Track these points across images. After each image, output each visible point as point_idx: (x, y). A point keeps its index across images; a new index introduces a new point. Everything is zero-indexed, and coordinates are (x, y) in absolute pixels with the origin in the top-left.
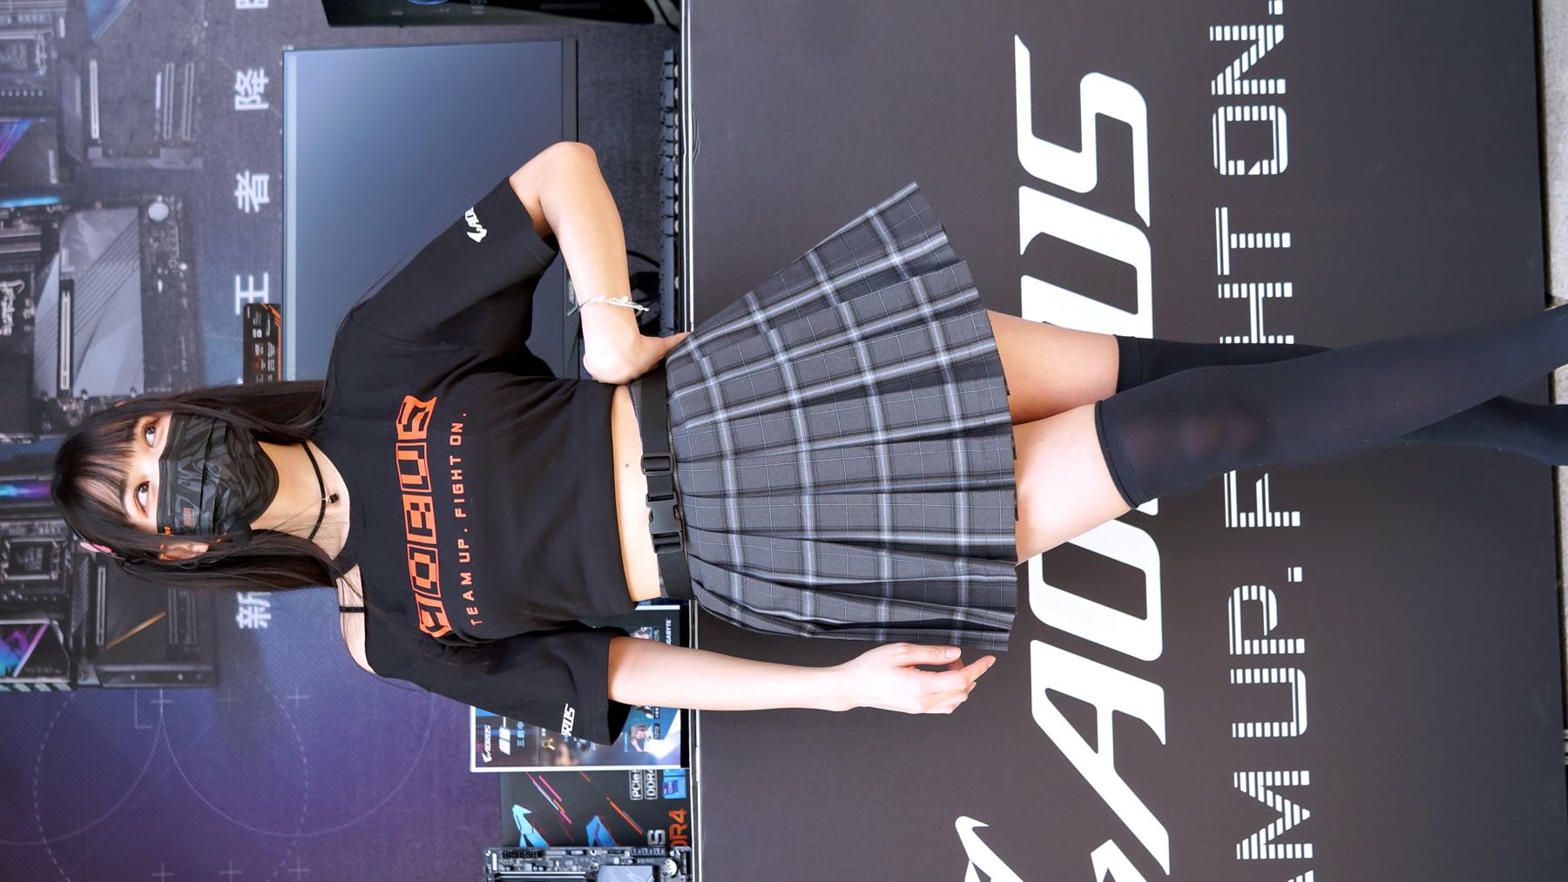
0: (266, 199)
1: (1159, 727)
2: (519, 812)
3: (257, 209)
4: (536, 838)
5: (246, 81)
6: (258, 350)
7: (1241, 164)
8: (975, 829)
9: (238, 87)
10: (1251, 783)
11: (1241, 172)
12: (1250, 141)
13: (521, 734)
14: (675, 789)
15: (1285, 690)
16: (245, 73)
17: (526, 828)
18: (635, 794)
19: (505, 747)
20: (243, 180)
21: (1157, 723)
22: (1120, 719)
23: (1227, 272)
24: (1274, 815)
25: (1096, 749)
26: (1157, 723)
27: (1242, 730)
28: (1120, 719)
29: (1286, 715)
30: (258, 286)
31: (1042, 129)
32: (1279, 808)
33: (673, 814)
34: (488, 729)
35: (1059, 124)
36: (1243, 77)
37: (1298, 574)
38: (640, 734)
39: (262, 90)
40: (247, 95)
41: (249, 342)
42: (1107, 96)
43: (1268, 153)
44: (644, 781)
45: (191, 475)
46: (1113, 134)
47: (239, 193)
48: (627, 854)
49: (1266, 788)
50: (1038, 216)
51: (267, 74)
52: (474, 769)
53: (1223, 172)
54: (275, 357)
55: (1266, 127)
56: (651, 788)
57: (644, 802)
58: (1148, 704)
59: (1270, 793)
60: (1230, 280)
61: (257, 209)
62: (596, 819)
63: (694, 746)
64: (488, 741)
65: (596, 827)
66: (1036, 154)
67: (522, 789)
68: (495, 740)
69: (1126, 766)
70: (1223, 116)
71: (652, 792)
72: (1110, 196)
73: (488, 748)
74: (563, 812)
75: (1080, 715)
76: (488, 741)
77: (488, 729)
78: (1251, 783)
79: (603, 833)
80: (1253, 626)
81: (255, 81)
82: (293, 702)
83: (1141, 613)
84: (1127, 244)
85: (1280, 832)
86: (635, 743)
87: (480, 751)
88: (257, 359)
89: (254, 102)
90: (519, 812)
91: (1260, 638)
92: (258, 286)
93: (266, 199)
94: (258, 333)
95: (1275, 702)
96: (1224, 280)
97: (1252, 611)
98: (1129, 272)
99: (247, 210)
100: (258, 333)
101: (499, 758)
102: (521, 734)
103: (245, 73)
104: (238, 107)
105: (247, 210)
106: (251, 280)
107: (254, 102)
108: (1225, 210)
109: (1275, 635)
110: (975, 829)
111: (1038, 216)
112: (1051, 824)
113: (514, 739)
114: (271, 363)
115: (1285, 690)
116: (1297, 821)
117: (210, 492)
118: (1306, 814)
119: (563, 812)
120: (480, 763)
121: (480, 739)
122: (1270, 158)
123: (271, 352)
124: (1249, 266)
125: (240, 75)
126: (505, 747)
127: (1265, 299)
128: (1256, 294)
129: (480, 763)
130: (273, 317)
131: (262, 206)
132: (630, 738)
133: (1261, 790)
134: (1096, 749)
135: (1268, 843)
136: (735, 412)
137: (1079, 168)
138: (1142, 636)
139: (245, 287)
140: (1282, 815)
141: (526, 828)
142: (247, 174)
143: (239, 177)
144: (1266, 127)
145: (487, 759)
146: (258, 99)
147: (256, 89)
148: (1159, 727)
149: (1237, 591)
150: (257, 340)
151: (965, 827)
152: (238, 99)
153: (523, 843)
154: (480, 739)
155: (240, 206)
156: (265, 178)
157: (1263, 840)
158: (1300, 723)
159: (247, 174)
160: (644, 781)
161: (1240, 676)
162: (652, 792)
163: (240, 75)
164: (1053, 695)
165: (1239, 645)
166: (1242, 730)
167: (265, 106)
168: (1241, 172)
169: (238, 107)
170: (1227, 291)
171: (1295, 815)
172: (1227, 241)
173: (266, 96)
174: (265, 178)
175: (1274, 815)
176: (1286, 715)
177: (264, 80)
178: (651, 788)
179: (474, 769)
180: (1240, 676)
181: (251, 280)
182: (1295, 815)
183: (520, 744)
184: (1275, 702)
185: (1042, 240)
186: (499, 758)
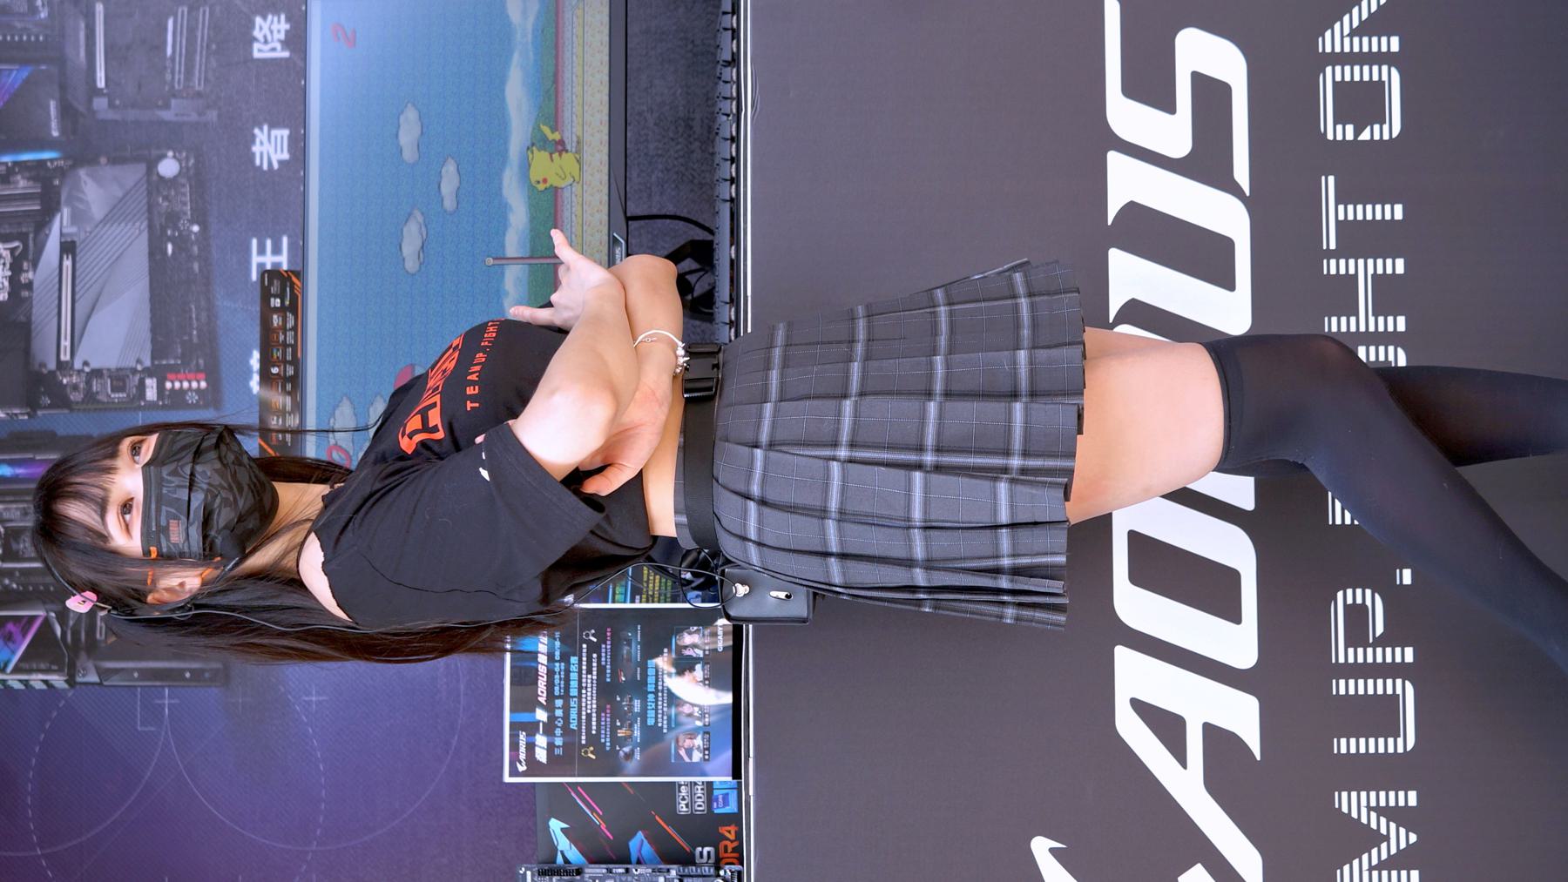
0: (286, 156)
1: (1253, 742)
2: (556, 825)
3: (276, 166)
4: (574, 855)
5: (266, 26)
6: (276, 320)
7: (1350, 128)
8: (1052, 851)
9: (256, 33)
10: (1354, 804)
11: (1350, 136)
12: (1361, 103)
13: (559, 742)
14: (726, 803)
15: (1392, 702)
16: (265, 18)
17: (563, 843)
18: (682, 808)
19: (541, 755)
20: (261, 134)
21: (1252, 738)
22: (1209, 729)
23: (1333, 246)
24: (1377, 838)
25: (1184, 764)
26: (1252, 738)
27: (1343, 746)
28: (1209, 729)
29: (1392, 728)
30: (277, 250)
31: (1130, 90)
32: (1383, 831)
33: (723, 830)
34: (522, 736)
35: (1151, 84)
36: (1353, 33)
37: (1407, 577)
38: (688, 743)
39: (282, 36)
40: (266, 42)
41: (266, 312)
42: (1203, 53)
43: (1378, 115)
44: (692, 794)
45: (176, 481)
46: (1211, 93)
47: (256, 149)
48: (673, 873)
49: (1369, 809)
50: (1126, 183)
51: (288, 20)
52: (507, 779)
53: (1330, 137)
54: (295, 328)
55: (1378, 88)
56: (700, 802)
57: (691, 817)
58: (1241, 715)
59: (1373, 815)
60: (1337, 254)
61: (276, 166)
62: (640, 835)
63: (747, 756)
64: (523, 749)
65: (639, 844)
66: (1126, 116)
67: (560, 800)
68: (531, 747)
69: (1214, 784)
70: (1330, 77)
71: (700, 805)
72: (1205, 164)
73: (522, 757)
74: (603, 826)
75: (1168, 727)
76: (523, 749)
77: (522, 736)
78: (1354, 804)
79: (647, 850)
80: (1357, 635)
81: (275, 27)
82: (309, 703)
83: (1235, 617)
84: (1224, 215)
85: (1384, 856)
86: (682, 752)
87: (514, 760)
88: (275, 331)
89: (274, 49)
90: (556, 825)
91: (1365, 645)
92: (277, 250)
93: (286, 156)
94: (276, 302)
95: (1382, 716)
96: (1330, 254)
97: (1357, 615)
98: (1227, 245)
99: (265, 167)
100: (276, 302)
101: (534, 767)
102: (559, 742)
103: (265, 18)
104: (256, 55)
105: (265, 167)
106: (269, 243)
107: (274, 49)
108: (1331, 179)
109: (1381, 642)
110: (1052, 851)
111: (1126, 183)
112: (1139, 854)
113: (551, 747)
114: (290, 335)
115: (1392, 702)
116: (1403, 845)
117: (198, 500)
118: (1413, 838)
119: (603, 826)
120: (514, 772)
121: (514, 746)
122: (1382, 123)
123: (290, 323)
124: (1357, 239)
125: (258, 20)
126: (541, 755)
127: (1375, 275)
128: (1364, 270)
129: (514, 772)
130: (293, 284)
131: (281, 162)
132: (678, 747)
133: (1364, 811)
134: (1184, 764)
135: (1371, 869)
136: (947, 459)
137: (1173, 132)
138: (1238, 644)
139: (262, 251)
140: (1387, 838)
141: (563, 843)
142: (266, 128)
143: (257, 131)
144: (1378, 88)
145: (522, 768)
146: (279, 46)
147: (276, 36)
148: (1253, 742)
149: (1340, 594)
150: (276, 310)
151: (1041, 847)
152: (256, 46)
153: (560, 860)
154: (514, 746)
155: (258, 162)
156: (286, 132)
157: (1365, 866)
158: (1409, 738)
159: (266, 128)
160: (692, 794)
161: (1342, 687)
162: (700, 805)
163: (258, 20)
164: (1139, 706)
165: (1342, 653)
166: (1343, 746)
167: (286, 54)
168: (1350, 136)
169: (256, 55)
170: (1332, 267)
171: (1401, 838)
172: (1333, 213)
173: (286, 44)
174: (286, 132)
175: (1377, 838)
176: (1392, 728)
177: (285, 26)
178: (700, 802)
179: (507, 779)
180: (1342, 687)
181: (269, 243)
182: (1401, 838)
183: (558, 752)
184: (1382, 716)
185: (1133, 210)
186: (534, 767)
